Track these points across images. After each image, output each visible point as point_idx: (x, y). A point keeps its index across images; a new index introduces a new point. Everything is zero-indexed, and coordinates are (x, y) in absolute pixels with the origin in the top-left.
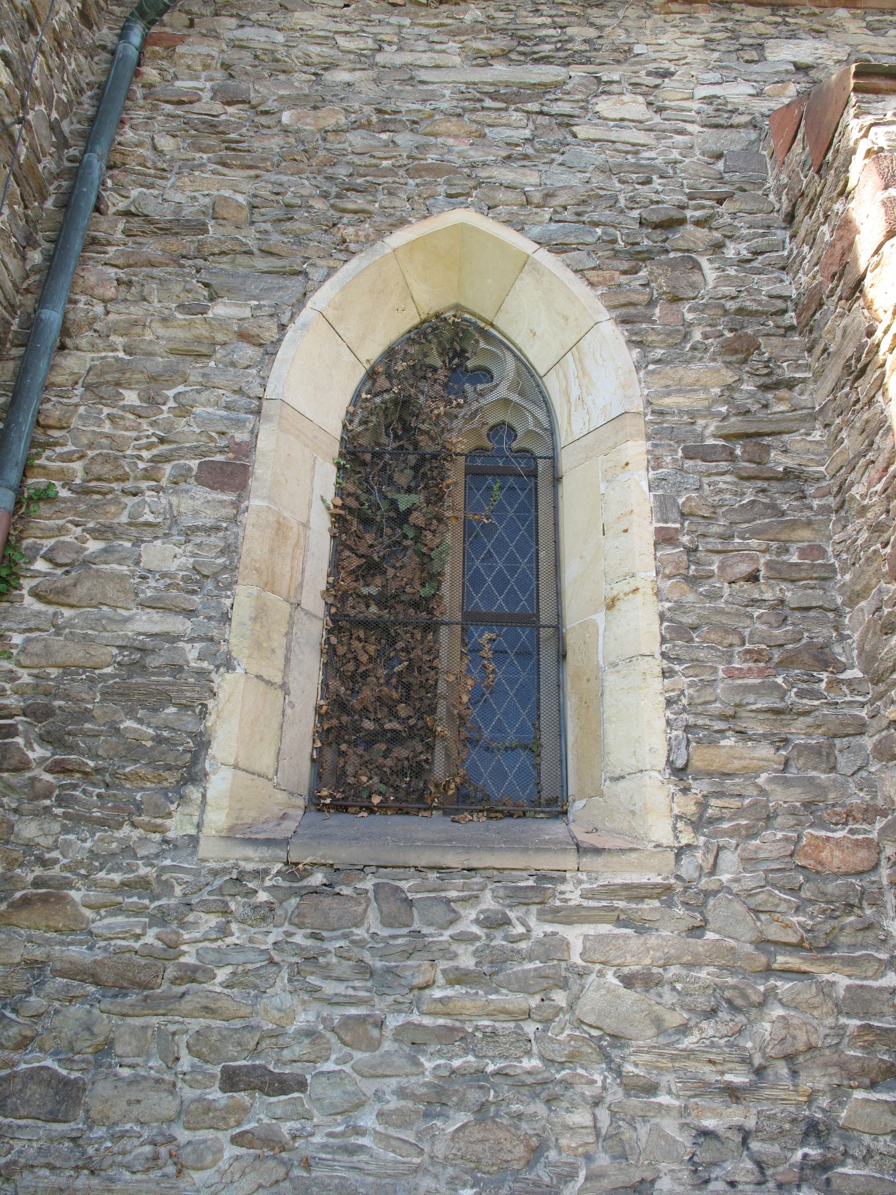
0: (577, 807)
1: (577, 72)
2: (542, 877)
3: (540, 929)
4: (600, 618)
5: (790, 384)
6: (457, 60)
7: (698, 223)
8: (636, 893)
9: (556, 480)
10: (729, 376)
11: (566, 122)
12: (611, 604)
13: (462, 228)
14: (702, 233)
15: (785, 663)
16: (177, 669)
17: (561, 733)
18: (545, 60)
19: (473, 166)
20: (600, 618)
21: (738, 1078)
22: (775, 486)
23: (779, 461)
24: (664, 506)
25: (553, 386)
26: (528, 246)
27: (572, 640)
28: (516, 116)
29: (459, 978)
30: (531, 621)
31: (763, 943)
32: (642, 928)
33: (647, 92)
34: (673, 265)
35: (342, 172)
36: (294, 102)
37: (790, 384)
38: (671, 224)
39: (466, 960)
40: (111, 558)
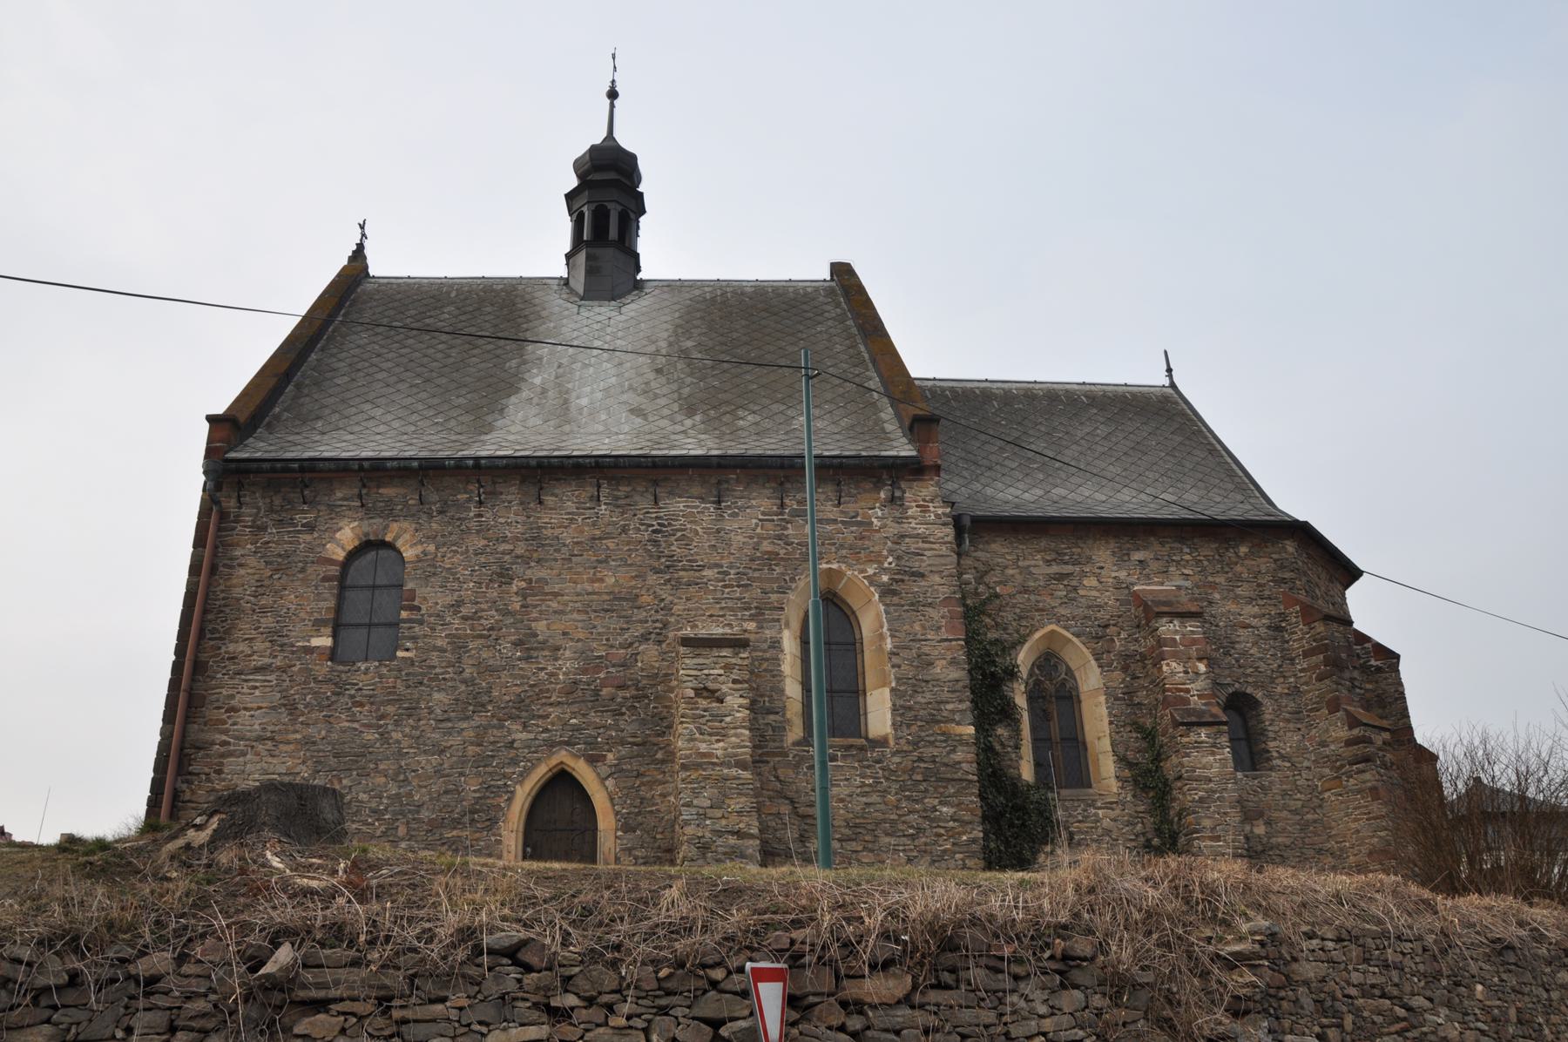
0: (1094, 785)
1: (1077, 569)
2: (1093, 801)
3: (1093, 811)
4: (1096, 742)
5: (1138, 678)
6: (1041, 563)
7: (1114, 625)
8: (1112, 803)
9: (1080, 702)
10: (1123, 676)
11: (1075, 589)
12: (1099, 738)
13: (1053, 632)
14: (1115, 628)
15: (1139, 752)
16: (1011, 760)
17: (1088, 769)
18: (1066, 563)
19: (1053, 608)
20: (1096, 742)
21: (1133, 837)
22: (1135, 708)
23: (1136, 700)
24: (1110, 714)
25: (1077, 674)
26: (1070, 636)
27: (1089, 746)
28: (1061, 586)
29: (1080, 822)
30: (1076, 739)
31: (1136, 812)
32: (1113, 809)
33: (1098, 576)
34: (1108, 641)
35: (1018, 611)
36: (1000, 583)
37: (1138, 678)
38: (1106, 626)
39: (1080, 818)
40: (717, 666)
